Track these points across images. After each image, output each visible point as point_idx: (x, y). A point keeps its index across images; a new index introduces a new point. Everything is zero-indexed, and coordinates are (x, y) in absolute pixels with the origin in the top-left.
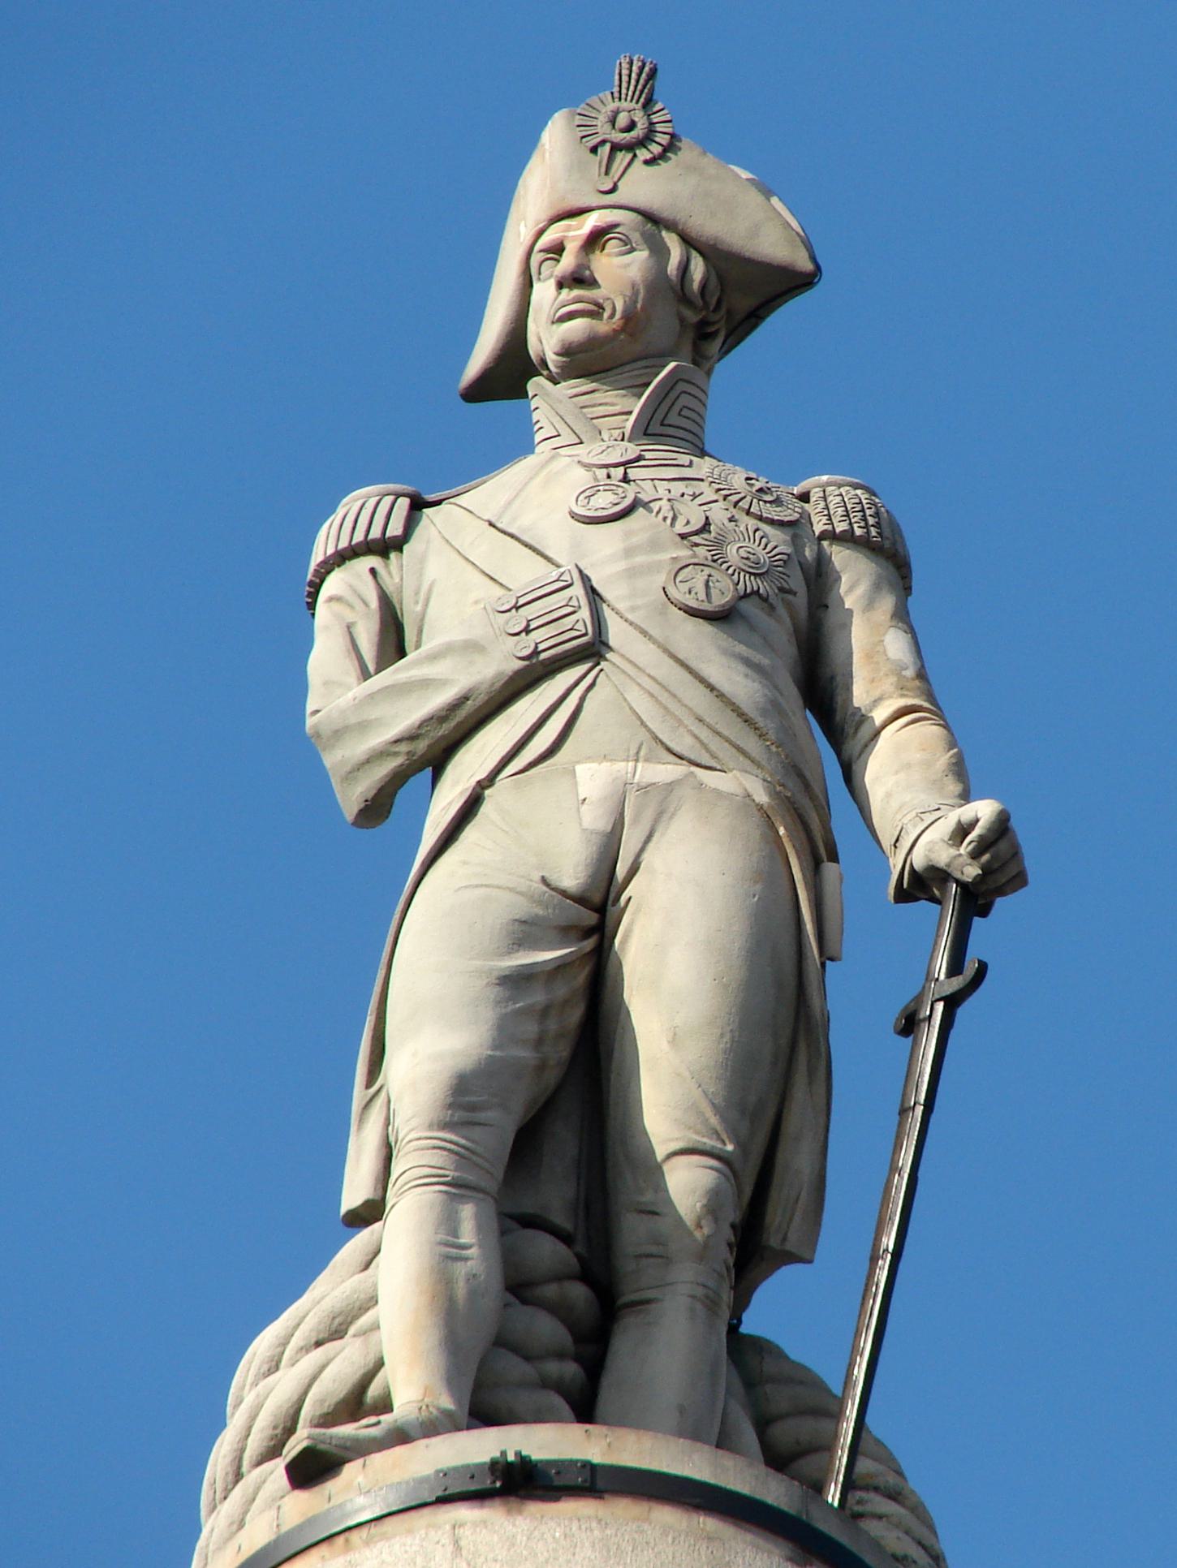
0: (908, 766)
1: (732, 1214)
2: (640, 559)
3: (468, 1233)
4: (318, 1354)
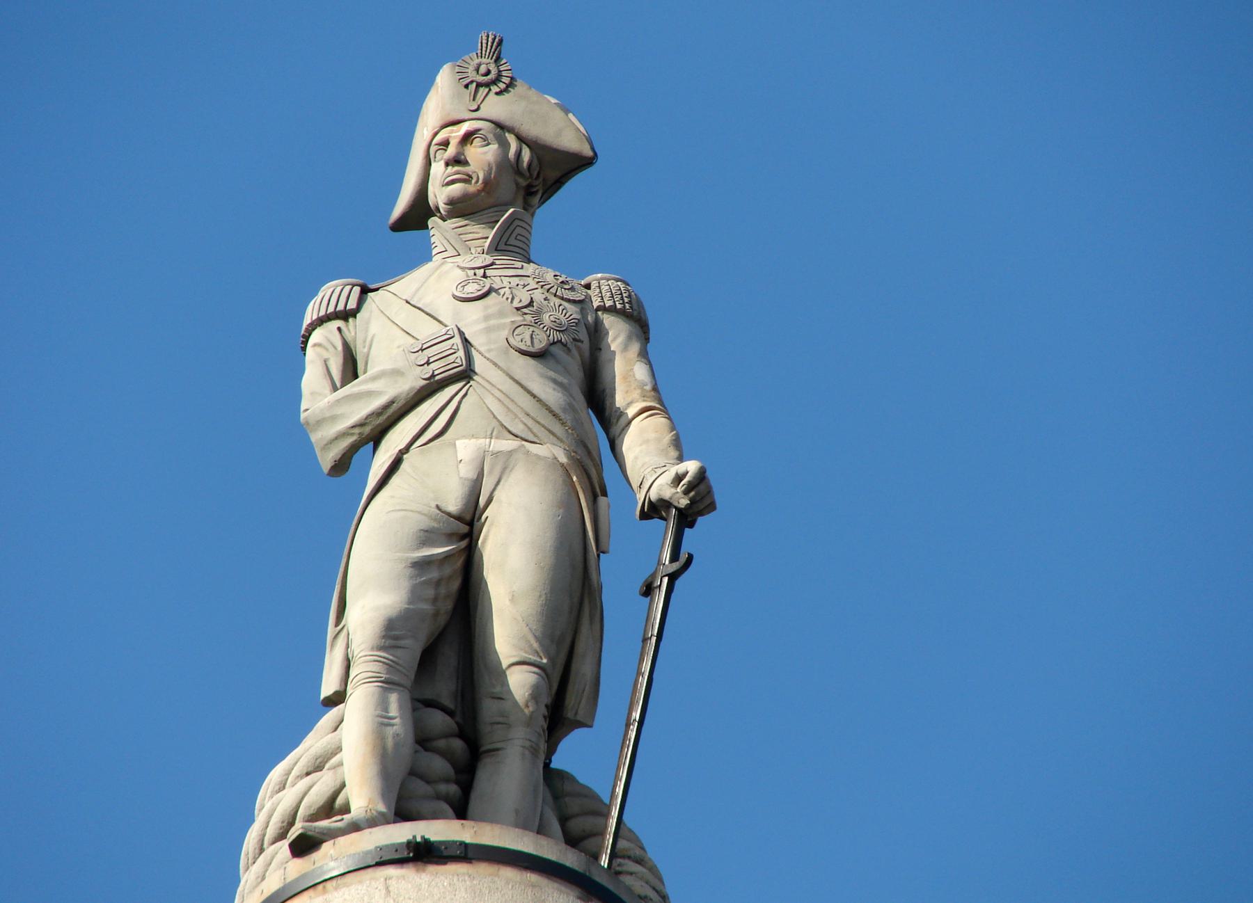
0: (647, 441)
1: (546, 699)
2: (493, 322)
3: (394, 710)
4: (308, 780)
